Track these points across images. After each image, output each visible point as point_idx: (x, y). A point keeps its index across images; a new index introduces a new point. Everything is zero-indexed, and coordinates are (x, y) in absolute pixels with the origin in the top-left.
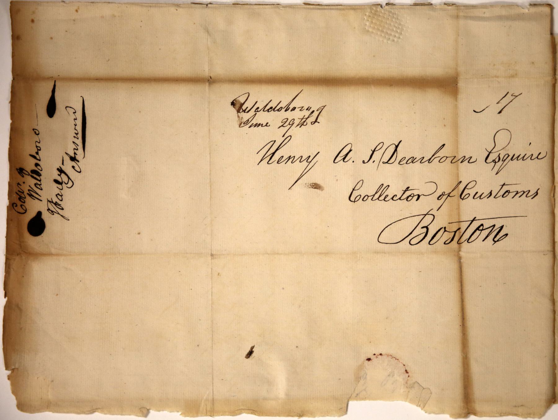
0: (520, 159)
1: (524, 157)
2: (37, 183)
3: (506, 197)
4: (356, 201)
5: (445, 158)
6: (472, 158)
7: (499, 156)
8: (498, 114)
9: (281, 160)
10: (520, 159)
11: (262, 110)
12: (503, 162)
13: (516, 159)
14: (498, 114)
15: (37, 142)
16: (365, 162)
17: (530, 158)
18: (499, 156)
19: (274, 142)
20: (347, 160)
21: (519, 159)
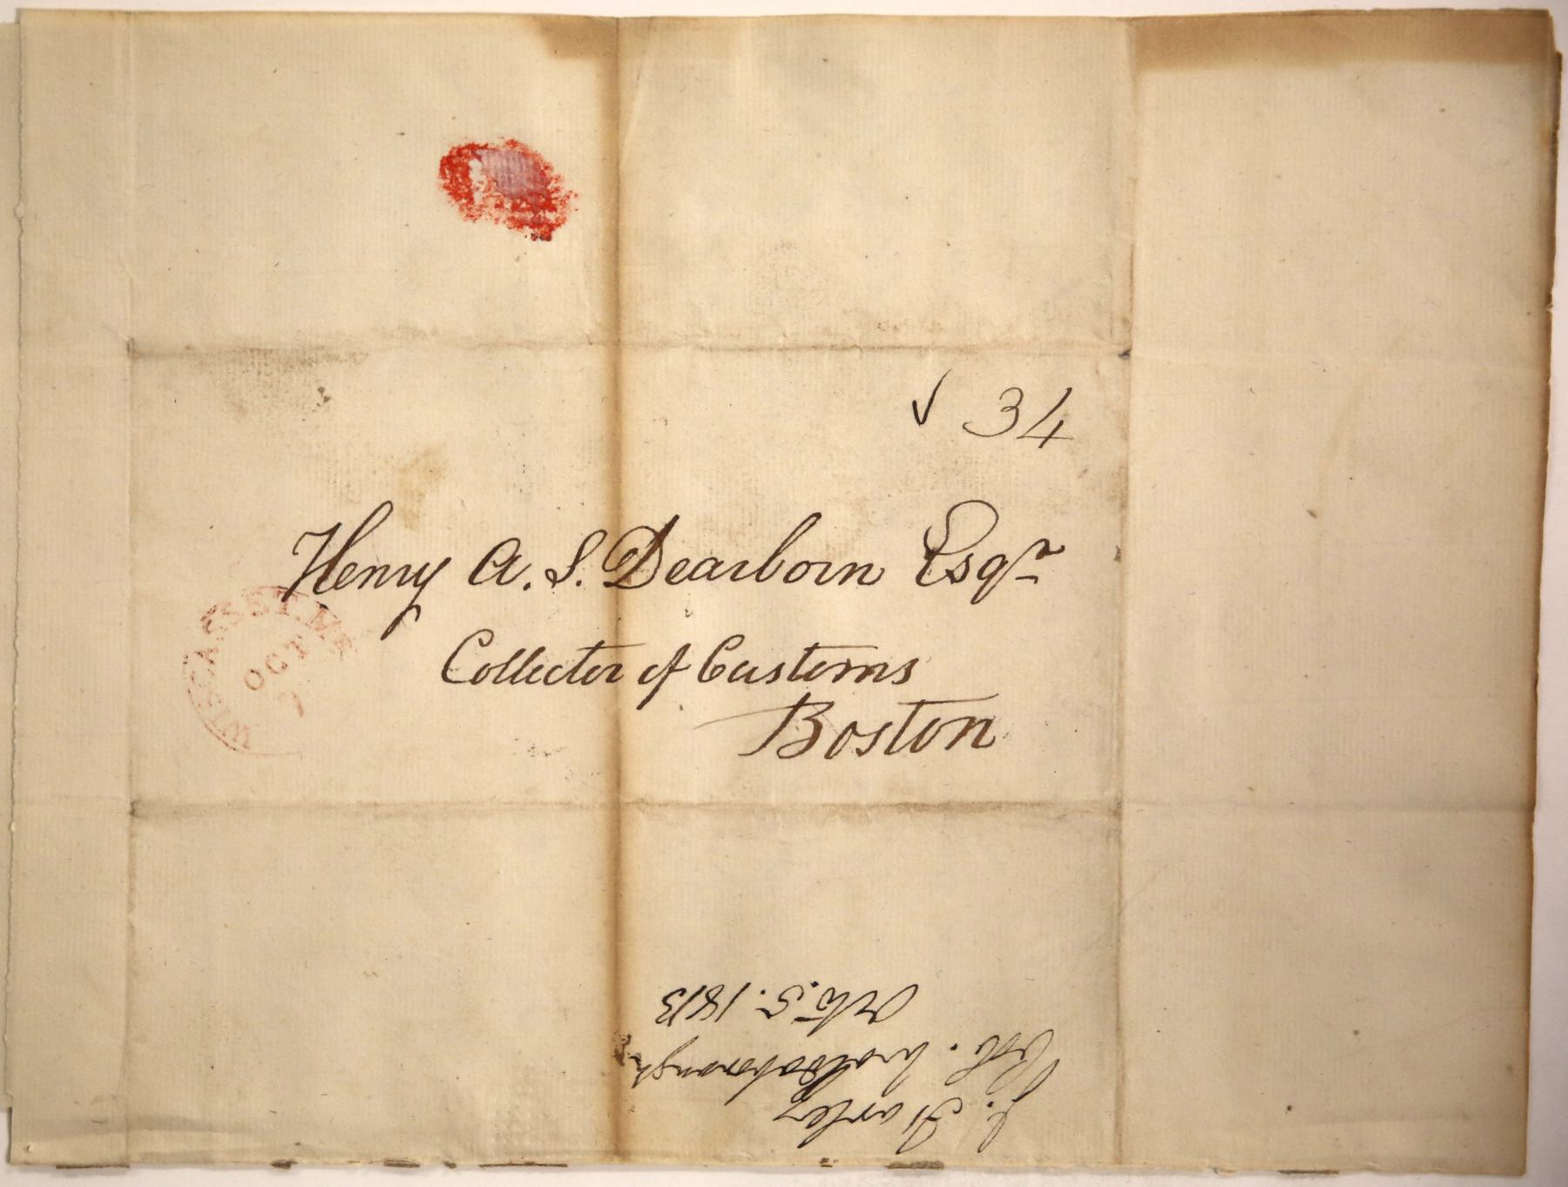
0: (840, 996)
1: (761, 570)
2: (1007, 562)
3: (846, 566)
4: (559, 581)
5: (804, 567)
6: (881, 1093)
7: (967, 561)
8: (1037, 559)
9: (678, 573)
10: (840, 996)
11: (731, 573)
12: (420, 591)
13: (754, 576)
14: (1037, 559)
15: (1021, 1053)
16: (560, 575)
17: (496, 578)
18: (967, 561)
19: (824, 566)
20: (511, 578)
21: (517, 679)
